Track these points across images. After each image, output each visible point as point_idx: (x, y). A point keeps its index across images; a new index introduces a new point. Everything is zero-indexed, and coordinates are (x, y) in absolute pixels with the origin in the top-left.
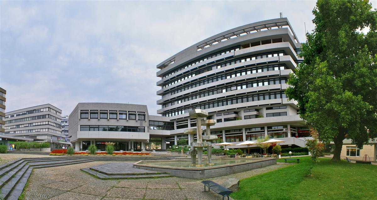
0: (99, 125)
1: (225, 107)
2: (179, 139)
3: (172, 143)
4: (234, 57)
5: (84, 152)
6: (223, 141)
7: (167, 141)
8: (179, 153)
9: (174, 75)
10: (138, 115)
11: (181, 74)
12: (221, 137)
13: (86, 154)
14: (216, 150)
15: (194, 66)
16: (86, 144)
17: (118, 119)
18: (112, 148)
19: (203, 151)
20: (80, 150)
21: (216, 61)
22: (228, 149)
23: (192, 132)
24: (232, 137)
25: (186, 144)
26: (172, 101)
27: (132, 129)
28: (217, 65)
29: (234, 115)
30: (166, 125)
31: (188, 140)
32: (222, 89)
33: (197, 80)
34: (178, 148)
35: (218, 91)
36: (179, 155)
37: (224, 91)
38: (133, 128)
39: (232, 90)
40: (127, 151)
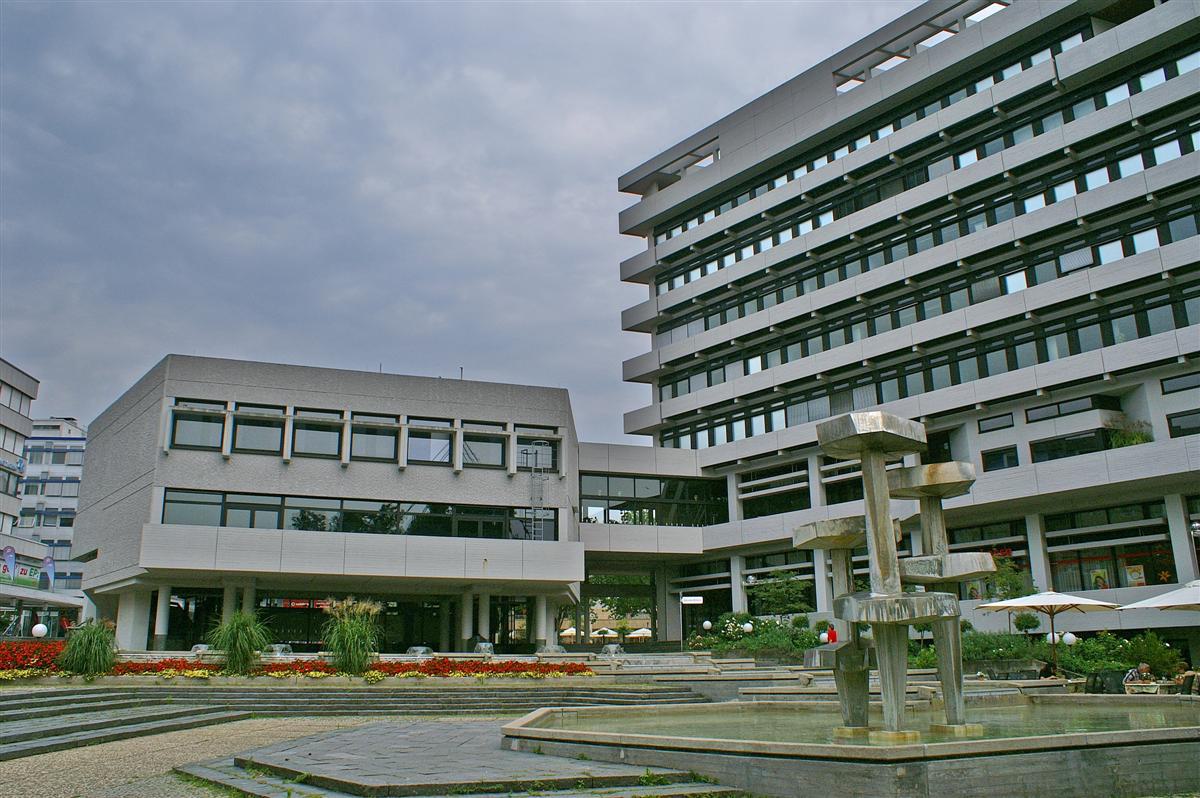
0: (283, 496)
1: (1031, 377)
2: (759, 576)
3: (719, 602)
4: (1053, 89)
5: (179, 655)
6: (1030, 580)
7: (690, 588)
8: (760, 661)
9: (714, 223)
10: (521, 440)
11: (757, 219)
12: (1017, 559)
13: (198, 673)
14: (985, 637)
15: (824, 170)
16: (192, 608)
17: (403, 462)
18: (363, 637)
19: (913, 652)
20: (150, 647)
21: (946, 130)
22: (1070, 638)
23: (842, 537)
24: (1095, 556)
25: (803, 606)
26: (713, 361)
27: (479, 519)
28: (957, 150)
29: (1094, 420)
30: (678, 493)
31: (813, 581)
32: (1002, 271)
33: (845, 240)
34: (754, 633)
35: (973, 286)
36: (761, 674)
37: (1016, 281)
38: (487, 518)
39: (1064, 269)
40: (452, 650)
